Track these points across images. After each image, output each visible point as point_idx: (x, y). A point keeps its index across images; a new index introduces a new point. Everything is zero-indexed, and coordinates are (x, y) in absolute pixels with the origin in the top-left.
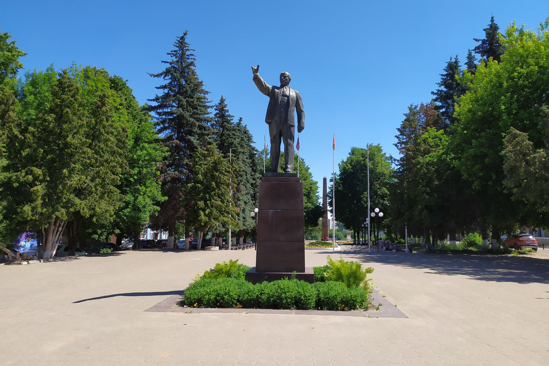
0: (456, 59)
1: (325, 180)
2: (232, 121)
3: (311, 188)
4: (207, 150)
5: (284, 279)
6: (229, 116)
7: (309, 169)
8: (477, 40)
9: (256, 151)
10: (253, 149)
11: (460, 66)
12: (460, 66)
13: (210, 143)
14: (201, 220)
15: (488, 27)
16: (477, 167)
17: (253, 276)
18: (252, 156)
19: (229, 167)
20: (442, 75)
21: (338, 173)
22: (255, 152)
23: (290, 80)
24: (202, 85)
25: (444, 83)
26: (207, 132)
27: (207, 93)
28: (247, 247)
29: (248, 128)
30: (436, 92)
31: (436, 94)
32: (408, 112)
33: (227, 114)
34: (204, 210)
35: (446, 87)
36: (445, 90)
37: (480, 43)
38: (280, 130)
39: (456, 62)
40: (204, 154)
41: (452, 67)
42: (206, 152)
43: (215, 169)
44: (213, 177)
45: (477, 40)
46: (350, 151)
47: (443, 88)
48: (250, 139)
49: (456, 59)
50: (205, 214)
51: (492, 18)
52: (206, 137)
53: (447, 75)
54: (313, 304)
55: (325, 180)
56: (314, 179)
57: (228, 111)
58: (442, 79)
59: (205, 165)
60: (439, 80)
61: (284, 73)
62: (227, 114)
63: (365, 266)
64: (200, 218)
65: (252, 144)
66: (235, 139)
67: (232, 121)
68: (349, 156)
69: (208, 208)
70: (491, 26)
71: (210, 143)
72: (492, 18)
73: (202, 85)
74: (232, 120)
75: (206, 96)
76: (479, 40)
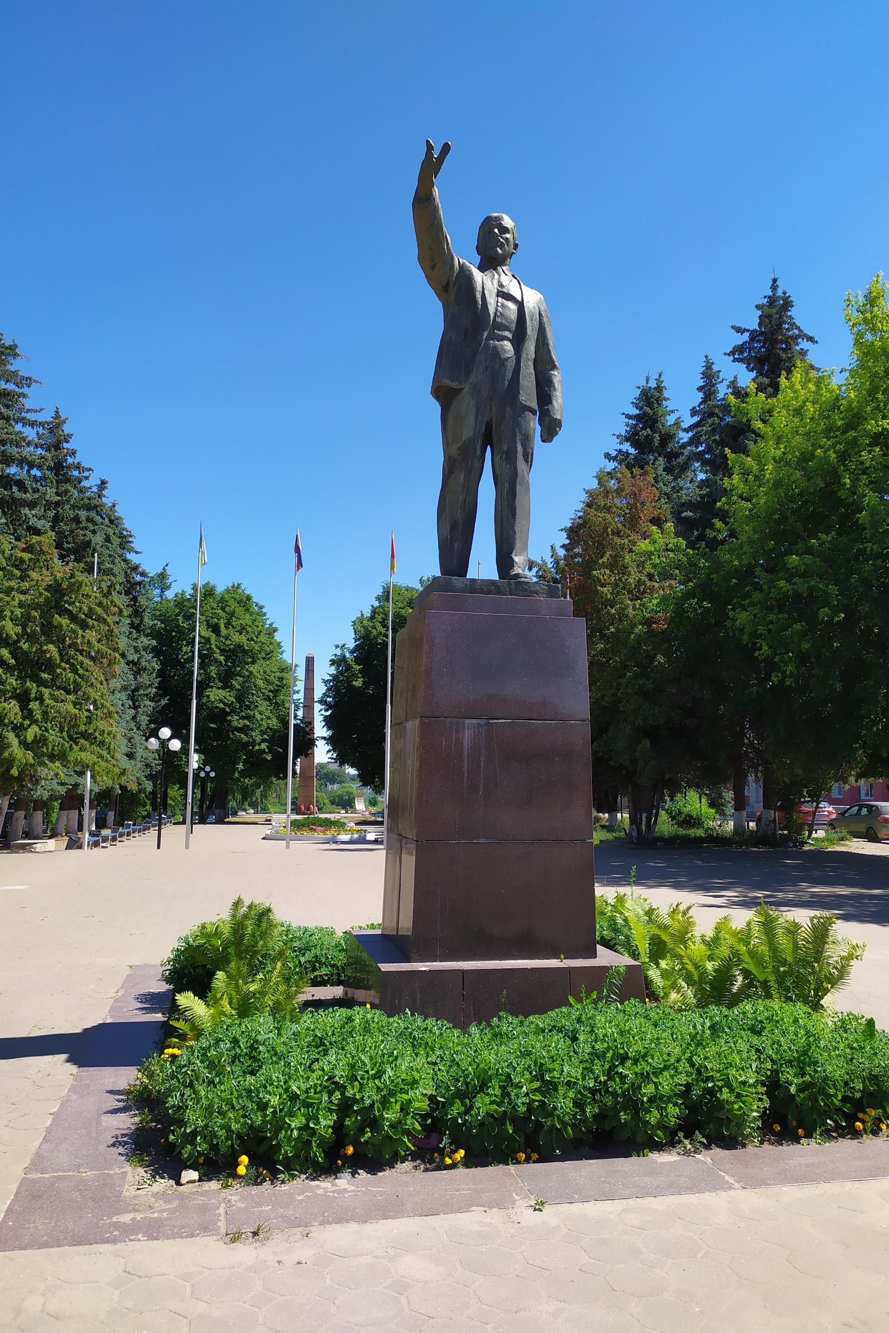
0: (659, 381)
1: (310, 661)
2: (85, 484)
3: (281, 679)
4: (29, 549)
5: (579, 1000)
6: (78, 467)
7: (275, 630)
8: (740, 330)
9: (143, 574)
10: (135, 568)
11: (666, 399)
12: (666, 399)
13: (37, 532)
14: (11, 762)
15: (765, 301)
16: (797, 626)
17: (359, 970)
18: (131, 588)
19: (100, 604)
20: (628, 417)
21: (351, 645)
22: (138, 578)
23: (516, 246)
24: (15, 355)
25: (632, 437)
26: (28, 496)
27: (29, 381)
28: (121, 835)
29: (120, 512)
30: (614, 454)
31: (615, 459)
32: (594, 484)
33: (70, 460)
34: (18, 729)
35: (635, 444)
36: (632, 451)
37: (746, 337)
38: (489, 426)
39: (659, 389)
40: (22, 560)
41: (650, 400)
42: (27, 556)
43: (56, 607)
44: (48, 629)
45: (740, 330)
46: (380, 591)
47: (627, 447)
48: (125, 541)
49: (659, 381)
50: (24, 744)
51: (775, 280)
52: (26, 511)
53: (637, 417)
54: (755, 1108)
55: (310, 661)
56: (287, 657)
57: (73, 453)
58: (627, 425)
59: (24, 593)
60: (623, 430)
61: (499, 219)
62: (70, 460)
63: (846, 933)
64: (6, 754)
65: (130, 556)
66: (94, 532)
67: (85, 484)
68: (376, 604)
69: (34, 722)
70: (772, 300)
71: (37, 532)
72: (775, 280)
73: (15, 355)
74: (87, 478)
75: (25, 390)
76: (746, 330)
